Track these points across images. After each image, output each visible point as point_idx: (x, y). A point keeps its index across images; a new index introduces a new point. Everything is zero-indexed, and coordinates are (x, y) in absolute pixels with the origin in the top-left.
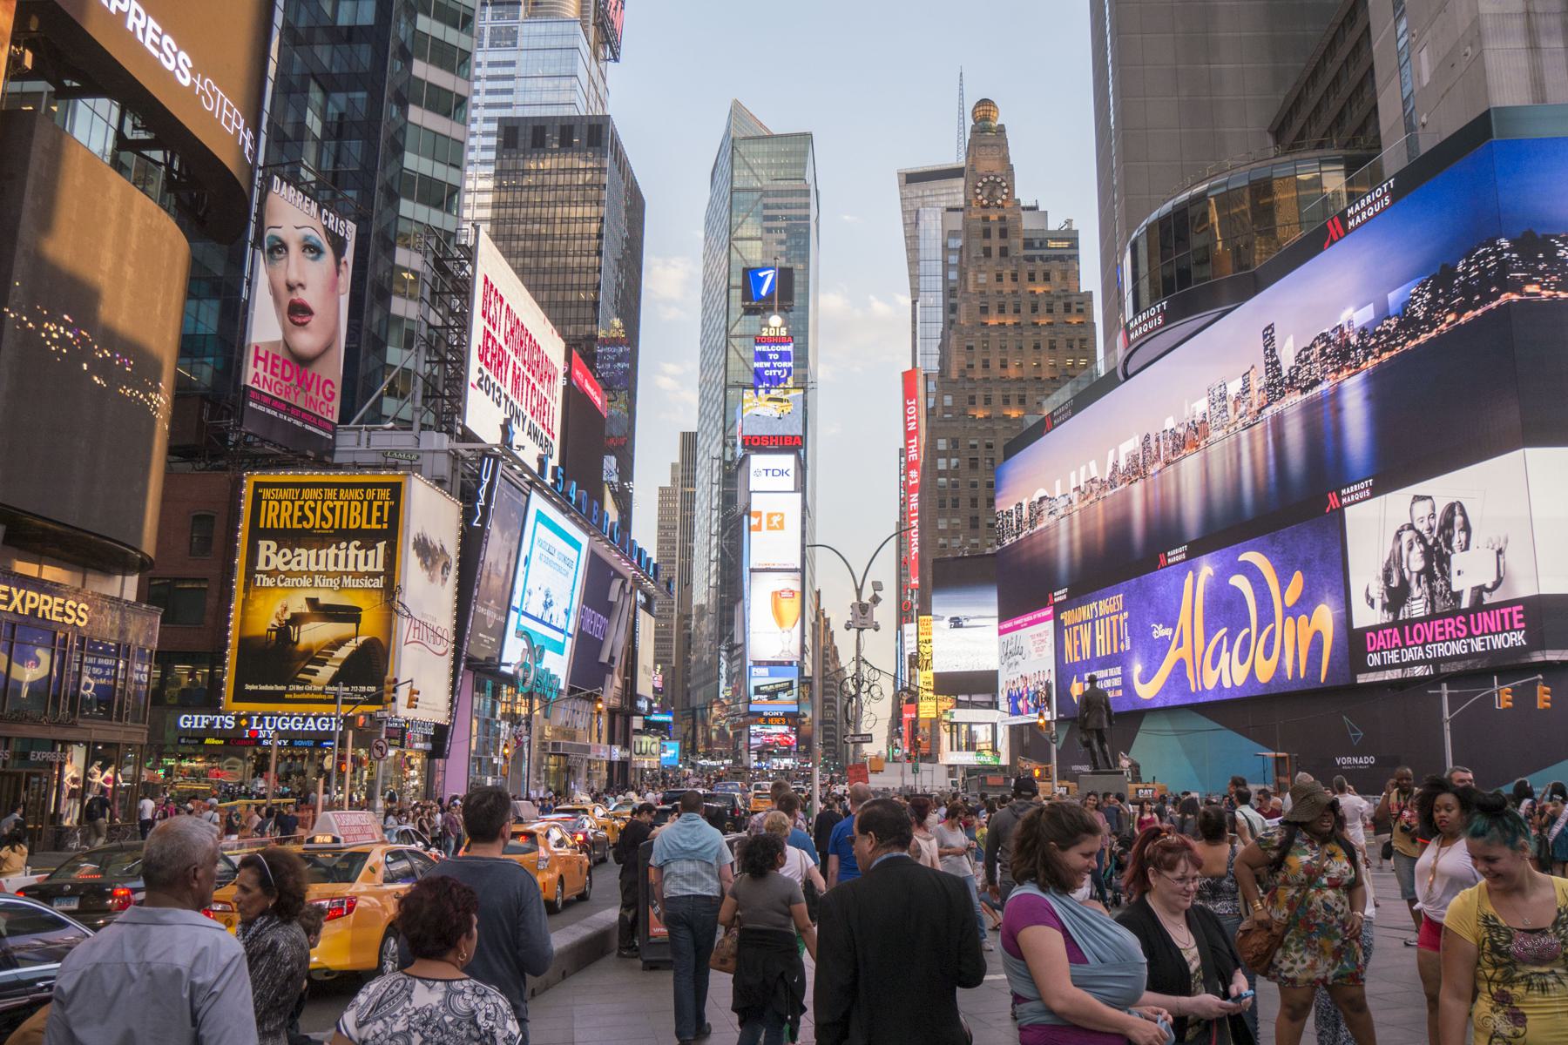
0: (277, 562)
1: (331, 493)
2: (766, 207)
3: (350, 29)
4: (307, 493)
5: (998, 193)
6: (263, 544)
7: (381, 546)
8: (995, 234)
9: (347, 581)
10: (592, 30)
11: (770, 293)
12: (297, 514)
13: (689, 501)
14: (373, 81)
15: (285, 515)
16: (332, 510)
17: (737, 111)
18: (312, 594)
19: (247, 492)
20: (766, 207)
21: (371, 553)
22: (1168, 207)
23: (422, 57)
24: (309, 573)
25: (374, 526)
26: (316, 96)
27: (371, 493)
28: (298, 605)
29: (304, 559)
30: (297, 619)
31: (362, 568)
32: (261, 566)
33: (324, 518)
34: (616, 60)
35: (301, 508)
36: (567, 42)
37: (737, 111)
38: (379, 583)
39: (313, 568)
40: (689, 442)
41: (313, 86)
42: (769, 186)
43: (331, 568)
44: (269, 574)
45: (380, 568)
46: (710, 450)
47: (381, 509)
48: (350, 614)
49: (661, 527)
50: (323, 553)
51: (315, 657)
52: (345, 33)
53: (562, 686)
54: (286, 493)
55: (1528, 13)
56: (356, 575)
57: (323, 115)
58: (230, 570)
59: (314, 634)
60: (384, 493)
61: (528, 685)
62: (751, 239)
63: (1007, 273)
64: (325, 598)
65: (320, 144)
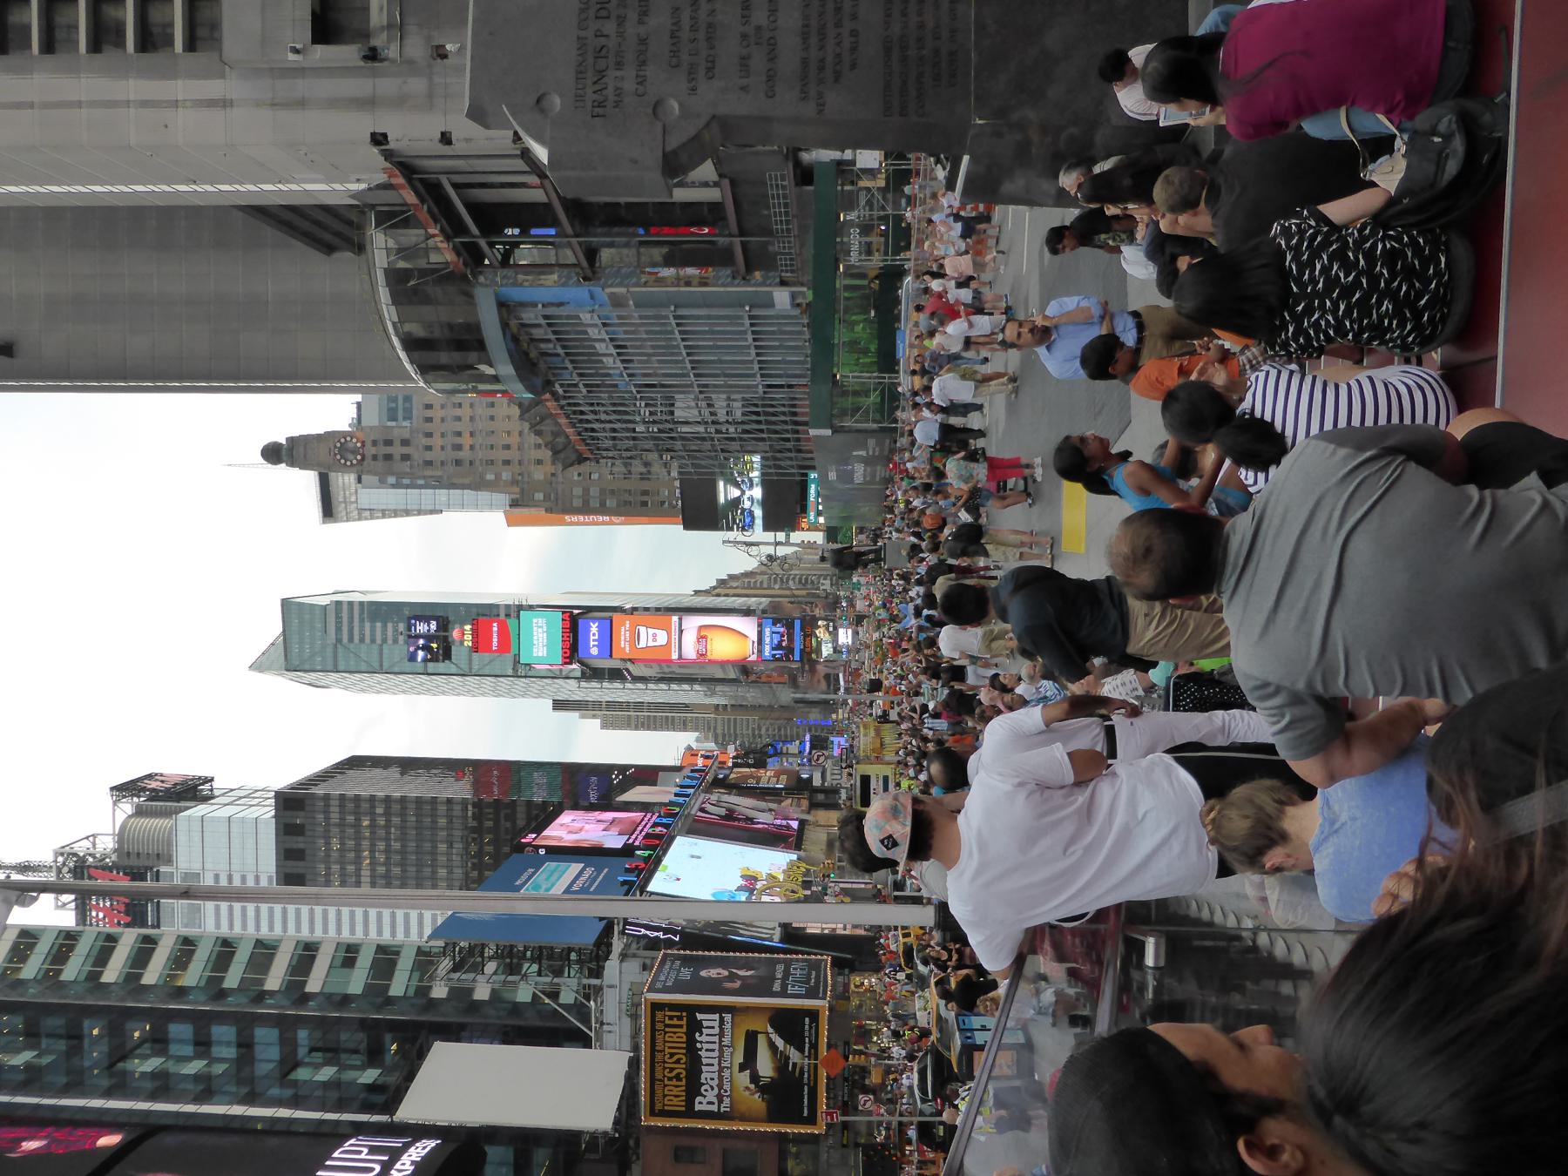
0: (711, 1096)
1: (659, 1056)
2: (351, 639)
3: (239, 1045)
4: (658, 1075)
5: (350, 445)
6: (698, 1107)
7: (699, 1016)
8: (389, 450)
9: (726, 1041)
10: (183, 804)
11: (437, 638)
12: (674, 1082)
13: (611, 705)
14: (116, 1019)
15: (676, 1091)
16: (672, 1055)
17: (259, 666)
18: (736, 1068)
19: (660, 1123)
20: (351, 639)
21: (705, 1024)
22: (402, 355)
23: (261, 982)
24: (721, 1070)
25: (684, 1022)
26: (302, 1074)
27: (659, 1026)
28: (744, 1078)
29: (709, 1076)
30: (755, 1078)
31: (717, 1030)
32: (714, 1108)
33: (678, 1061)
34: (212, 780)
35: (670, 1079)
36: (197, 826)
37: (259, 666)
38: (728, 1017)
39: (716, 1068)
40: (559, 705)
41: (293, 1076)
42: (325, 639)
43: (716, 1054)
44: (720, 1101)
45: (716, 1016)
46: (572, 689)
47: (671, 1018)
48: (751, 1038)
49: (637, 728)
50: (705, 1061)
51: (781, 1062)
52: (243, 1050)
53: (794, 857)
54: (659, 1092)
55: (273, 105)
56: (721, 1034)
57: (318, 1067)
58: (715, 1133)
59: (765, 1067)
60: (659, 1015)
61: (795, 887)
62: (381, 654)
63: (426, 441)
64: (739, 1058)
65: (343, 1067)
